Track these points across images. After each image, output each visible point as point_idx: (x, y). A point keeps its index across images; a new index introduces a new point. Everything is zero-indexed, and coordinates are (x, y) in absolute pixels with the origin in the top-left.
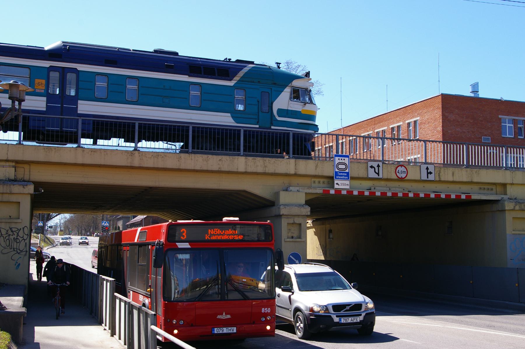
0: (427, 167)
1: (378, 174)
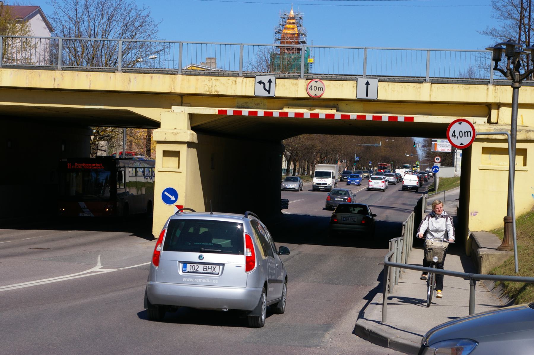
0: (258, 82)
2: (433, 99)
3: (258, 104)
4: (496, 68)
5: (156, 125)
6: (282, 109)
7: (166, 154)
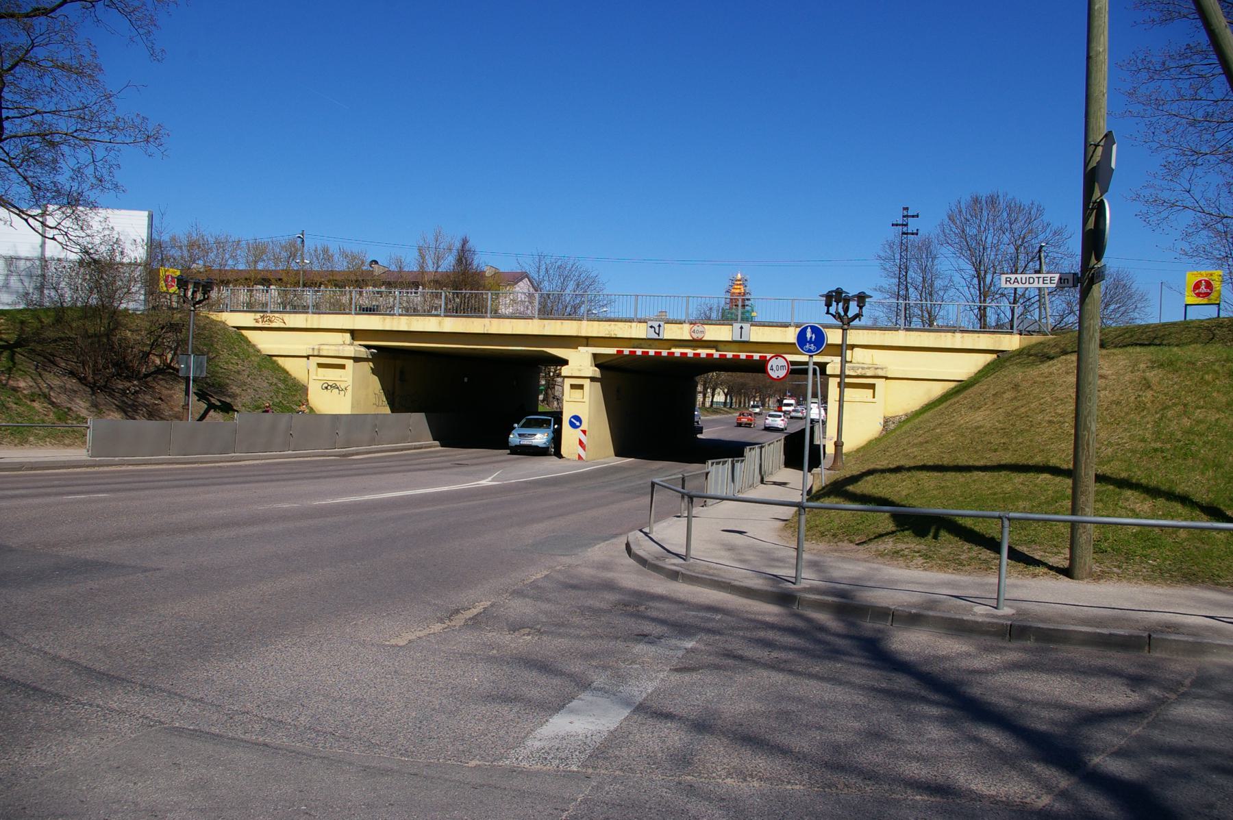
1: (659, 334)
3: (650, 345)
4: (828, 313)
5: (565, 362)
6: (670, 349)
7: (573, 387)
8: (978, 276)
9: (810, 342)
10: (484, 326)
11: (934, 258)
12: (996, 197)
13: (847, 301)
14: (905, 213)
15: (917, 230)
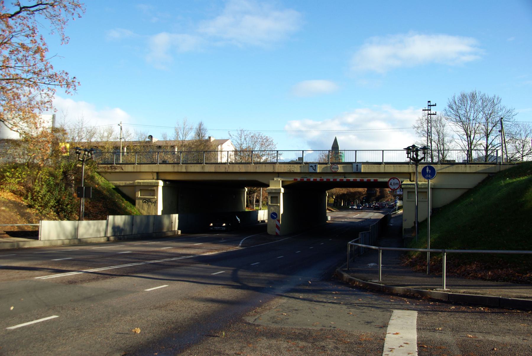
2: (386, 171)
8: (467, 135)
9: (429, 174)
10: (226, 168)
11: (443, 126)
12: (474, 94)
13: (417, 150)
14: (429, 104)
15: (436, 112)
